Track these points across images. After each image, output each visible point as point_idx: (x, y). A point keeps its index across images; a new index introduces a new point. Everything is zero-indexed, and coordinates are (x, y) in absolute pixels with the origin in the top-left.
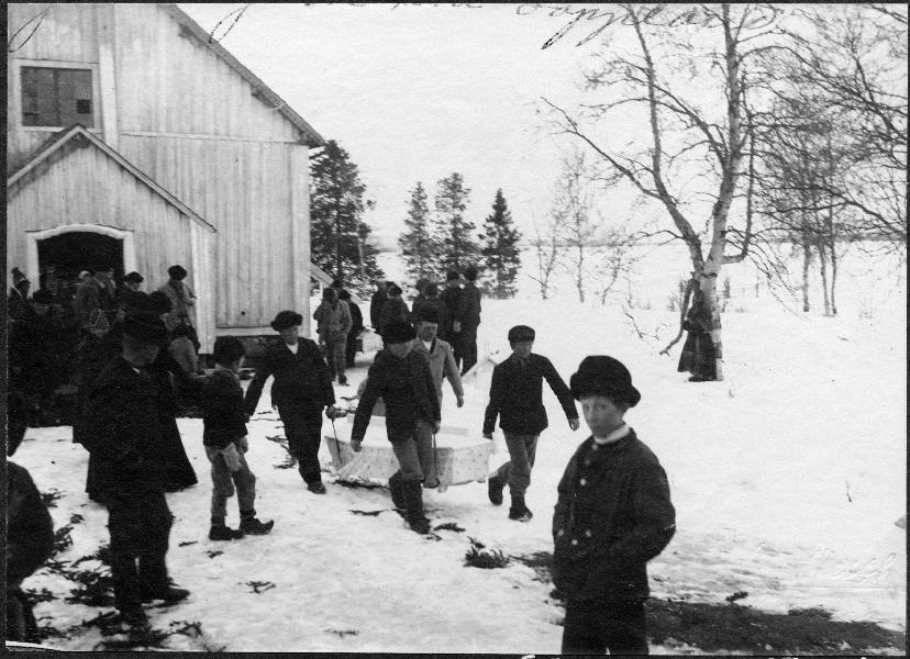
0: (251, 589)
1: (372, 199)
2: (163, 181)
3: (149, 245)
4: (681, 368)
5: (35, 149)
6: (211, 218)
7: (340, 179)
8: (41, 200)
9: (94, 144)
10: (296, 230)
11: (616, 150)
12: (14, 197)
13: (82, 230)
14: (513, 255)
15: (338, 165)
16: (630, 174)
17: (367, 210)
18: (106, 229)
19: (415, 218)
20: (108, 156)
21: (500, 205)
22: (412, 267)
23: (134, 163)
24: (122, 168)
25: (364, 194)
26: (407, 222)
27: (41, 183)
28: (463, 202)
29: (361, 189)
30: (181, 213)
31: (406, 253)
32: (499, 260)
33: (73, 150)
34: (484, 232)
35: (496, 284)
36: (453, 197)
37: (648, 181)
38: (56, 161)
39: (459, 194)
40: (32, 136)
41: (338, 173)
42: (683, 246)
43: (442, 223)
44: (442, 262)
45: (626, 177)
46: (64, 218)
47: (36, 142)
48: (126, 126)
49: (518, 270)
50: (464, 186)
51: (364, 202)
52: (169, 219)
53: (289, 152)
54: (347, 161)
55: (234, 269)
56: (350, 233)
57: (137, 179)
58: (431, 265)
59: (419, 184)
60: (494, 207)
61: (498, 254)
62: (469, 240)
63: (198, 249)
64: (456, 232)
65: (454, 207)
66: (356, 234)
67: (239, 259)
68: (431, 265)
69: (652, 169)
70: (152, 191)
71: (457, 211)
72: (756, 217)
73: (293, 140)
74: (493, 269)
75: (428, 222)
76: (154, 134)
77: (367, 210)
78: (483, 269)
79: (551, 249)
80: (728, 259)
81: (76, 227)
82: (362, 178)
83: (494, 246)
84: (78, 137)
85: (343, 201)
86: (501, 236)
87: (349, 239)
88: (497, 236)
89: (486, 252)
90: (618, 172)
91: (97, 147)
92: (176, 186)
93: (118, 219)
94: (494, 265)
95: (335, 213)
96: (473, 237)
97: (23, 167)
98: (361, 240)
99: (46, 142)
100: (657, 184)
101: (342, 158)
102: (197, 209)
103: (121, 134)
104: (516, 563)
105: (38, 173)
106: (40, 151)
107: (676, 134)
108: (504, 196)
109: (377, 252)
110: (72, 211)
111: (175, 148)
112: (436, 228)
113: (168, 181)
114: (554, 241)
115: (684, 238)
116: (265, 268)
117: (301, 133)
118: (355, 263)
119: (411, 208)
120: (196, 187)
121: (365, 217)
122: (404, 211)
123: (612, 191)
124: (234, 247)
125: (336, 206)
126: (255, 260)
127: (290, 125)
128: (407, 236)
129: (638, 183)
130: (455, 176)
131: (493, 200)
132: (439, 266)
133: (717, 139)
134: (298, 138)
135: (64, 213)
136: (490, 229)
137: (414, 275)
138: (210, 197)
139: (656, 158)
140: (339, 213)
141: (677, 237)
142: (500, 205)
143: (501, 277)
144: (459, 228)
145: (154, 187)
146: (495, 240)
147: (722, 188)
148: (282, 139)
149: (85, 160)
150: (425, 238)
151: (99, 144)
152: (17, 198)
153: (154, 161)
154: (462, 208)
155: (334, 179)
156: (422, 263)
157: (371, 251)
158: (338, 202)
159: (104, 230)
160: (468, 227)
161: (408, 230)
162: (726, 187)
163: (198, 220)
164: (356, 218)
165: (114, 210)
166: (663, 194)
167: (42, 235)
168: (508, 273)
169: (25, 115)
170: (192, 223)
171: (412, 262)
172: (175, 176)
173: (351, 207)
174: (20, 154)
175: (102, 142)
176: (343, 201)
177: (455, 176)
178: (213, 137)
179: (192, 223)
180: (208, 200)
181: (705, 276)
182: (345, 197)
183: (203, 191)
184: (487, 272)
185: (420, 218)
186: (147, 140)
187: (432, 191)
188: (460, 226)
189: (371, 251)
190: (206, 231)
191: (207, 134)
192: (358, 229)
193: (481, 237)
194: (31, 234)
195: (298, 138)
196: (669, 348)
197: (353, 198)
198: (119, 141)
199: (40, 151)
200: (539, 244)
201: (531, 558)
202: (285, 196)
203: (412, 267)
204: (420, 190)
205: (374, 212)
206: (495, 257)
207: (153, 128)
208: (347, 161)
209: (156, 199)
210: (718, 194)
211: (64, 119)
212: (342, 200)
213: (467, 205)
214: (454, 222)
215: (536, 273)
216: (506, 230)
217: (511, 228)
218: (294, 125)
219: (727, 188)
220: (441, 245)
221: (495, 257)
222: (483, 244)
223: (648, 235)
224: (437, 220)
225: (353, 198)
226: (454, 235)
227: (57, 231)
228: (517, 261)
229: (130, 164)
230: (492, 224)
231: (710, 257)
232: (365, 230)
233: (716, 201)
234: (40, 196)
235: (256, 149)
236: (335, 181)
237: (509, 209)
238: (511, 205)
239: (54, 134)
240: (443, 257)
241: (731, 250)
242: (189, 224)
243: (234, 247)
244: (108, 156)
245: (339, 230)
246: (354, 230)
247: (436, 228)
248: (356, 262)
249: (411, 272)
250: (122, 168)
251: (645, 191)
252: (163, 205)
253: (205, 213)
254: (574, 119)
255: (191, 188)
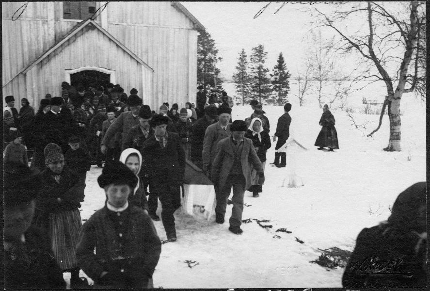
0: (187, 265)
1: (221, 57)
2: (128, 46)
3: (123, 74)
4: (316, 145)
5: (69, 30)
6: (150, 65)
7: (206, 47)
8: (72, 56)
9: (98, 28)
10: (190, 72)
11: (351, 35)
12: (60, 53)
13: (91, 70)
14: (286, 85)
15: (206, 40)
16: (357, 46)
17: (219, 61)
18: (101, 69)
19: (241, 66)
20: (104, 34)
21: (281, 60)
22: (239, 89)
23: (115, 37)
24: (110, 40)
25: (217, 54)
26: (237, 68)
27: (72, 47)
28: (264, 59)
29: (216, 52)
30: (138, 62)
31: (236, 82)
32: (279, 87)
33: (87, 31)
34: (273, 73)
35: (277, 98)
36: (259, 56)
37: (366, 50)
38: (80, 36)
39: (262, 55)
40: (68, 24)
41: (206, 44)
42: (383, 83)
43: (254, 68)
44: (253, 87)
45: (354, 48)
46: (83, 64)
47: (69, 27)
48: (111, 19)
49: (288, 92)
50: (264, 51)
51: (217, 58)
52: (133, 66)
53: (188, 33)
54: (210, 39)
55: (160, 89)
56: (211, 73)
57: (117, 45)
58: (247, 88)
59: (243, 49)
60: (278, 61)
61: (280, 84)
62: (266, 77)
63: (145, 79)
64: (260, 73)
65: (259, 61)
66: (213, 73)
67: (163, 84)
68: (247, 88)
69: (368, 44)
70: (124, 51)
71: (261, 63)
72: (419, 69)
73: (189, 28)
74: (277, 91)
75: (247, 68)
76: (124, 24)
77: (219, 61)
78: (272, 90)
79: (305, 82)
80: (406, 91)
81: (88, 68)
82: (217, 47)
83: (277, 80)
84: (90, 25)
85: (207, 57)
86: (281, 75)
87: (209, 76)
88: (279, 75)
89: (273, 83)
90: (351, 45)
91: (98, 30)
92: (134, 48)
93: (107, 65)
94: (277, 89)
95: (203, 63)
96: (268, 75)
97: (64, 38)
98: (215, 76)
99: (74, 27)
100: (370, 52)
101: (207, 37)
102: (144, 60)
103: (109, 23)
104: (199, 242)
105: (71, 41)
106: (72, 31)
107: (382, 28)
108: (283, 56)
109: (222, 82)
110: (86, 60)
111: (134, 30)
112: (250, 70)
113: (131, 47)
114: (306, 78)
115: (384, 79)
116: (175, 89)
117: (194, 24)
118: (212, 86)
119: (239, 61)
120: (144, 50)
121: (218, 65)
122: (235, 62)
123: (347, 55)
124: (161, 79)
125: (204, 60)
126: (170, 85)
127: (189, 20)
128: (237, 75)
129: (361, 52)
130: (260, 46)
131: (277, 58)
132: (252, 89)
133: (404, 29)
134: (193, 27)
135: (83, 62)
136: (276, 72)
137: (239, 93)
138: (150, 54)
139: (370, 40)
140: (205, 63)
141: (380, 79)
142: (281, 60)
143: (280, 95)
144: (261, 71)
145: (125, 49)
146: (278, 77)
147: (405, 55)
148: (185, 27)
149: (93, 35)
150: (245, 75)
151: (99, 28)
152: (61, 53)
153: (124, 35)
154: (263, 61)
155: (203, 46)
156: (244, 87)
157: (220, 81)
158: (205, 58)
159: (101, 70)
160: (265, 71)
161: (237, 72)
162: (407, 55)
163: (146, 66)
164: (213, 65)
165: (106, 60)
166: (373, 57)
167: (73, 72)
168: (283, 93)
169: (65, 13)
170: (143, 67)
171: (239, 87)
172: (134, 44)
173: (211, 60)
174: (62, 32)
175: (101, 27)
176: (207, 57)
177: (260, 46)
178: (152, 25)
179: (143, 67)
180: (149, 56)
181: (394, 98)
182: (209, 55)
183: (147, 52)
184: (274, 92)
185: (243, 66)
186: (121, 26)
187: (249, 53)
188: (262, 70)
189: (220, 81)
190: (149, 71)
191: (149, 24)
192: (214, 71)
193: (272, 75)
194: (67, 71)
195: (193, 27)
196: (372, 133)
197: (212, 56)
198: (108, 27)
199: (72, 31)
200: (299, 79)
201: (330, 250)
202: (186, 55)
203: (239, 89)
204: (243, 52)
205: (222, 62)
206: (277, 85)
207: (124, 21)
208: (210, 39)
209: (126, 55)
210: (403, 58)
211: (83, 15)
212: (207, 57)
213: (265, 60)
214: (259, 68)
215: (297, 93)
216: (284, 73)
217: (286, 71)
218: (191, 21)
219: (408, 56)
220: (252, 79)
221: (277, 85)
222: (273, 79)
223: (366, 78)
224: (251, 67)
225: (212, 56)
226: (259, 74)
227: (79, 70)
228: (288, 87)
229: (114, 38)
230: (277, 70)
231: (398, 89)
232: (217, 71)
233: (402, 61)
234: (72, 53)
235: (172, 31)
236: (204, 48)
237: (285, 63)
238: (286, 61)
239: (78, 23)
240: (253, 85)
241: (408, 86)
242: (141, 67)
243: (161, 79)
244: (104, 34)
245: (205, 71)
246: (212, 71)
247: (250, 70)
248: (213, 85)
249: (238, 91)
250: (110, 40)
251: (366, 56)
252: (129, 58)
253: (148, 62)
254: (331, 19)
255: (141, 50)
